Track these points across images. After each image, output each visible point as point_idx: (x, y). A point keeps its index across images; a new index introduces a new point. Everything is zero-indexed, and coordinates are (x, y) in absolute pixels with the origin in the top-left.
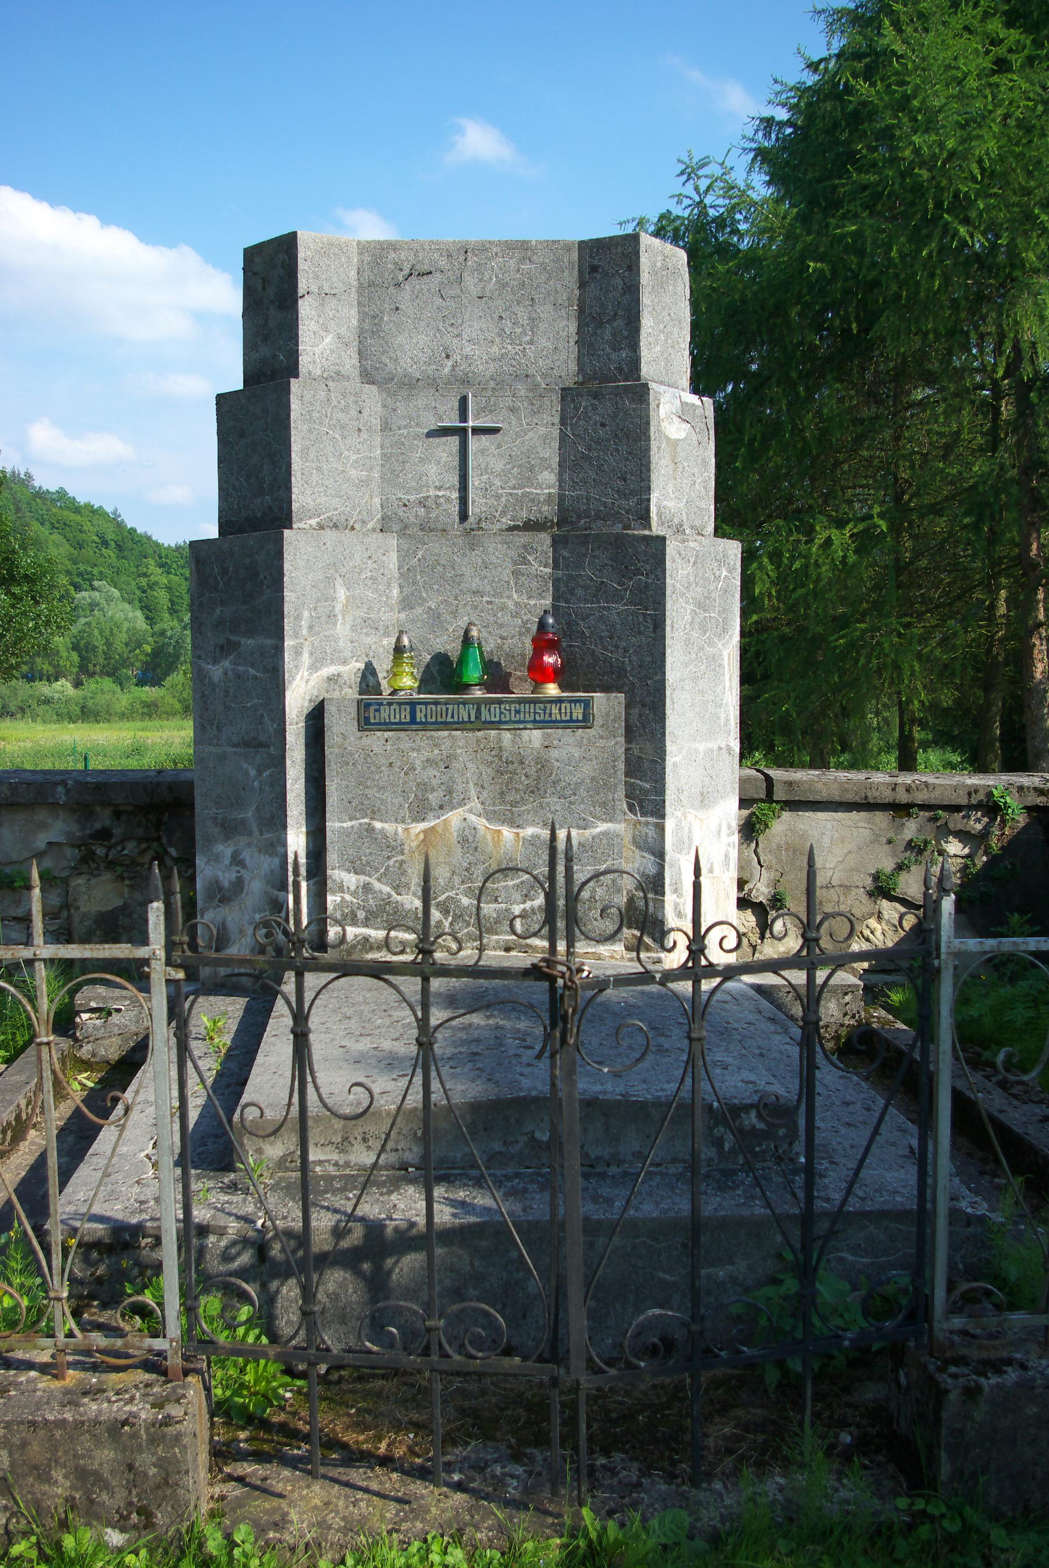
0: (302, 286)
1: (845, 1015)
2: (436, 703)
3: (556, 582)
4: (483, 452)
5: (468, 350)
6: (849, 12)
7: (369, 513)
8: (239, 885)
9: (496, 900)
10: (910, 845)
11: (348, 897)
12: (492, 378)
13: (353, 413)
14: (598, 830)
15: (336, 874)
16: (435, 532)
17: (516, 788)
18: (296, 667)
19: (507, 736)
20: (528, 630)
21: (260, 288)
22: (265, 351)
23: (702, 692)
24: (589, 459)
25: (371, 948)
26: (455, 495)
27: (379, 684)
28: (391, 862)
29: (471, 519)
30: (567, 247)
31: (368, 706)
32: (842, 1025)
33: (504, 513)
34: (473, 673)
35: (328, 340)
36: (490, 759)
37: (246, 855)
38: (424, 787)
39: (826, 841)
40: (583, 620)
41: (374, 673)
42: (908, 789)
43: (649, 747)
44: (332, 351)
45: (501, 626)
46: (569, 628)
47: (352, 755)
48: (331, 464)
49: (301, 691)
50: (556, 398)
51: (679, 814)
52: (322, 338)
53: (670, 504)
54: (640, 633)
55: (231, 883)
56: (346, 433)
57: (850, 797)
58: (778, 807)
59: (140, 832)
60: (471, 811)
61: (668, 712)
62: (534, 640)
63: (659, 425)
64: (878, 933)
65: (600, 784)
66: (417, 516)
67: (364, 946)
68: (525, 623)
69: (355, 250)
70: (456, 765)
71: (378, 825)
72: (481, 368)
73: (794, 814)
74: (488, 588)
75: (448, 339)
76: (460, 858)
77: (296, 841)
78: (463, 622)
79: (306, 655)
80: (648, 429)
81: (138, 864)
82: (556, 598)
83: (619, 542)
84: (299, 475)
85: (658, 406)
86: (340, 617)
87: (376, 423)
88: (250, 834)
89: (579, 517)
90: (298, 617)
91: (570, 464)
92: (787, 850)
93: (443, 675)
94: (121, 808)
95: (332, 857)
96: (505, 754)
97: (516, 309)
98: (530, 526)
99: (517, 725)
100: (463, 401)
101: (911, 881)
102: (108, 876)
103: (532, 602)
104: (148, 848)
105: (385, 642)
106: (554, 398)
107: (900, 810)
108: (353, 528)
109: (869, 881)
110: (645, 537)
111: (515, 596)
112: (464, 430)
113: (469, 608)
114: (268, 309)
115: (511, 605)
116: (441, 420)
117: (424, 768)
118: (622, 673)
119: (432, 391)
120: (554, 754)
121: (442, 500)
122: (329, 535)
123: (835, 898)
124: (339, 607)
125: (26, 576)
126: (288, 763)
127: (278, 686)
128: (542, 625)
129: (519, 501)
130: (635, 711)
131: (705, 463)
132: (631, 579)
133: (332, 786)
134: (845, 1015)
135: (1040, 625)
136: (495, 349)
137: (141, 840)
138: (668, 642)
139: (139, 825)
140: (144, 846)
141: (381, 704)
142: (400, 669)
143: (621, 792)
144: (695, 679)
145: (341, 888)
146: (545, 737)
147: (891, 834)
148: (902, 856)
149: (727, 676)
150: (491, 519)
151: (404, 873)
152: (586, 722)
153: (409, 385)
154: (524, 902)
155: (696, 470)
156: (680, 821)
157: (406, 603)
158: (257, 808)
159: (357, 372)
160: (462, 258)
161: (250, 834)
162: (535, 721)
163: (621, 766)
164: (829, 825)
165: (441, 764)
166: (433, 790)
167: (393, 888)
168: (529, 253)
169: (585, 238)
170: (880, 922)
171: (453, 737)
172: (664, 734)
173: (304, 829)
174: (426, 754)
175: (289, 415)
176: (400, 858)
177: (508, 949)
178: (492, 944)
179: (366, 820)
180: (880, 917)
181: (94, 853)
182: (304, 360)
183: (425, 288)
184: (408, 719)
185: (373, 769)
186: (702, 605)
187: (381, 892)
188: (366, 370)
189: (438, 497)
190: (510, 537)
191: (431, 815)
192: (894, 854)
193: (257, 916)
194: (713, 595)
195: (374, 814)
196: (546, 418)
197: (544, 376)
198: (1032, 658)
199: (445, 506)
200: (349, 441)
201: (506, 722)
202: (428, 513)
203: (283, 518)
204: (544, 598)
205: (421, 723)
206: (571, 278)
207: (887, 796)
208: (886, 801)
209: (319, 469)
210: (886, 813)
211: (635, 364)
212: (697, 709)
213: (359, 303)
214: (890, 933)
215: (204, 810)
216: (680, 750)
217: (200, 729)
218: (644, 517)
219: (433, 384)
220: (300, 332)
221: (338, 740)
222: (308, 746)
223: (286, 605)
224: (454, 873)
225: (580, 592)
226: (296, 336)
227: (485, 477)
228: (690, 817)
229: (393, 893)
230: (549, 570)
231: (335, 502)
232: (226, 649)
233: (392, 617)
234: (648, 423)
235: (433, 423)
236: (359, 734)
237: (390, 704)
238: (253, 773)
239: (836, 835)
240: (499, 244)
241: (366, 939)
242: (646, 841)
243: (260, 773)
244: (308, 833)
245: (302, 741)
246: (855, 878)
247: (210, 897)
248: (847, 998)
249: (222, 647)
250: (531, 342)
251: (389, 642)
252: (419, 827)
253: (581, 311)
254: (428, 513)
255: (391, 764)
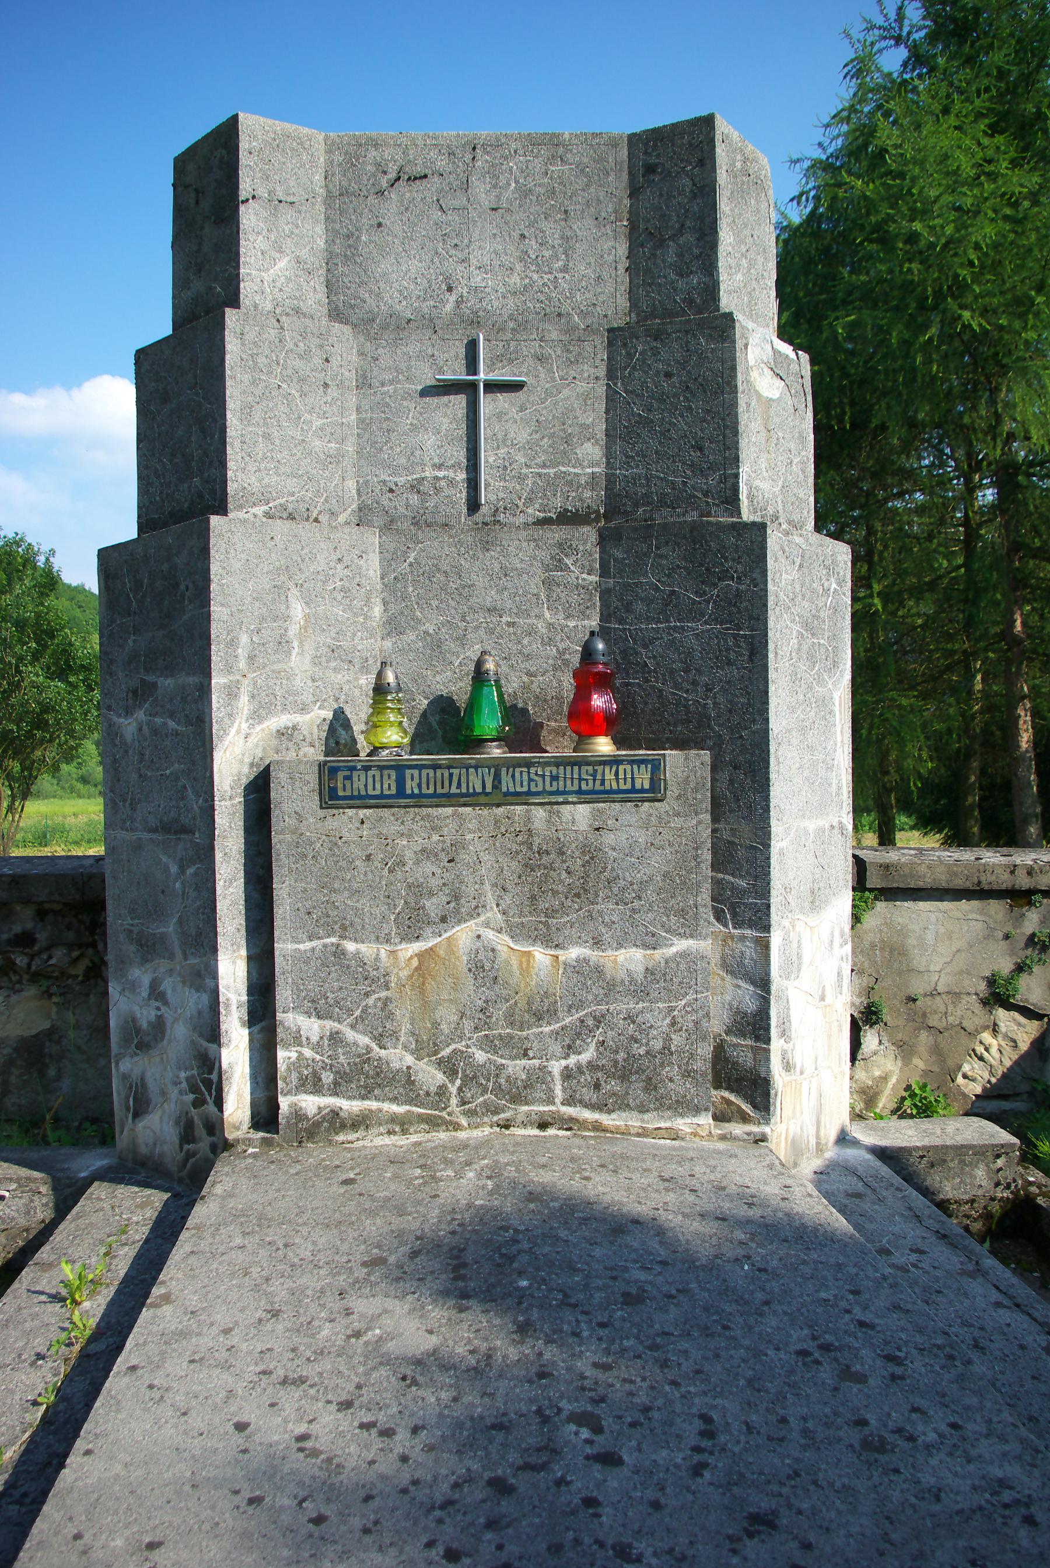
0: (245, 187)
1: (997, 1184)
2: (435, 767)
3: (605, 594)
4: (500, 416)
5: (478, 280)
6: (821, 162)
7: (340, 500)
8: (159, 1026)
9: (525, 1055)
10: (1031, 941)
11: (308, 1053)
12: (511, 317)
13: (317, 361)
14: (674, 950)
15: (291, 1018)
16: (432, 526)
17: (557, 890)
18: (230, 715)
19: (539, 814)
20: (566, 663)
21: (192, 202)
22: (198, 285)
23: (811, 748)
24: (648, 423)
25: (343, 1127)
26: (462, 476)
27: (354, 741)
28: (371, 1001)
29: (484, 510)
30: (613, 143)
31: (334, 771)
32: (993, 1199)
33: (530, 500)
34: (489, 723)
35: (282, 264)
36: (515, 847)
37: (167, 986)
38: (419, 890)
39: (930, 937)
40: (645, 646)
41: (347, 725)
42: (1030, 872)
43: (745, 827)
44: (289, 280)
45: (528, 657)
46: (625, 656)
47: (311, 844)
48: (285, 429)
49: (238, 750)
50: (600, 342)
51: (786, 923)
52: (275, 258)
53: (764, 485)
54: (729, 663)
55: (149, 1023)
56: (306, 388)
57: (959, 883)
58: (872, 896)
59: (70, 936)
60: (487, 925)
61: (773, 776)
62: (576, 675)
63: (748, 374)
64: (994, 1050)
65: (675, 883)
66: (407, 506)
67: (332, 1123)
68: (561, 653)
69: (322, 147)
70: (463, 857)
71: (350, 946)
72: (496, 304)
73: (890, 904)
74: (509, 604)
75: (451, 266)
76: (470, 992)
77: (232, 971)
78: (474, 653)
79: (244, 699)
80: (734, 377)
81: (69, 976)
82: (605, 617)
83: (696, 536)
84: (237, 444)
85: (746, 346)
86: (296, 644)
87: (350, 377)
88: (171, 957)
89: (636, 505)
90: (233, 643)
91: (621, 432)
92: (882, 949)
93: (446, 726)
94: (47, 906)
95: (283, 994)
96: (537, 841)
97: (544, 225)
98: (567, 518)
99: (554, 798)
100: (472, 347)
101: (1033, 985)
102: (31, 991)
103: (572, 624)
104: (82, 956)
105: (363, 681)
106: (598, 341)
107: (1020, 897)
108: (316, 520)
109: (982, 986)
110: (734, 526)
111: (547, 615)
112: (474, 385)
113: (481, 632)
114: (202, 228)
115: (541, 626)
116: (441, 371)
117: (417, 862)
118: (703, 720)
119: (429, 333)
120: (609, 839)
121: (443, 483)
122: (281, 528)
123: (942, 1009)
124: (293, 630)
125: (83, 666)
126: (219, 856)
127: (204, 745)
128: (588, 652)
129: (551, 483)
130: (725, 775)
131: (802, 439)
132: (715, 585)
133: (283, 890)
134: (997, 1184)
135: (1024, 697)
136: (515, 280)
137: (71, 947)
138: (772, 675)
139: (69, 927)
140: (75, 954)
141: (354, 768)
142: (382, 718)
143: (705, 896)
144: (803, 730)
145: (297, 1039)
146: (597, 814)
147: (1008, 928)
148: (1022, 954)
149: (838, 728)
150: (511, 508)
151: (390, 1016)
152: (655, 792)
153: (398, 327)
154: (566, 1057)
155: (792, 446)
156: (788, 934)
157: (393, 626)
158: (180, 922)
159: (325, 311)
160: (468, 157)
161: (171, 957)
162: (580, 792)
163: (707, 856)
164: (933, 917)
165: (442, 855)
166: (431, 894)
167: (374, 1038)
168: (561, 150)
169: (637, 130)
170: (995, 1037)
171: (460, 816)
172: (767, 809)
173: (244, 952)
174: (419, 843)
175: (223, 360)
176: (383, 994)
177: (543, 1126)
178: (520, 1118)
179: (333, 940)
180: (995, 1030)
181: (14, 964)
182: (246, 288)
183: (419, 197)
184: (393, 791)
185: (343, 864)
186: (810, 627)
187: (355, 1043)
188: (337, 308)
189: (437, 478)
190: (540, 532)
191: (429, 931)
192: (1012, 953)
193: (183, 1075)
194: (822, 614)
195: (344, 931)
196: (588, 370)
197: (583, 315)
198: (1018, 729)
199: (447, 492)
200: (310, 400)
201: (538, 794)
202: (424, 501)
203: (216, 500)
204: (589, 618)
205: (412, 796)
206: (618, 183)
207: (1004, 881)
208: (1004, 887)
209: (267, 436)
210: (1003, 902)
211: (712, 291)
212: (806, 773)
213: (327, 218)
214: (1007, 1050)
215: (117, 918)
216: (787, 830)
217: (112, 808)
218: (732, 500)
219: (431, 324)
220: (242, 250)
221: (291, 821)
222: (248, 830)
223: (213, 625)
224: (463, 1015)
225: (639, 607)
226: (237, 254)
227: (502, 451)
228: (800, 926)
229: (374, 1046)
230: (594, 578)
231: (291, 484)
232: (142, 693)
233: (373, 645)
234: (734, 368)
235: (428, 377)
236: (321, 813)
237: (366, 769)
238: (174, 869)
239: (942, 930)
240: (519, 137)
241: (335, 1113)
242: (741, 964)
243: (182, 870)
244: (250, 958)
245: (239, 823)
246: (966, 983)
247: (126, 1041)
248: (1000, 1162)
249: (135, 692)
250: (565, 269)
251: (367, 681)
252: (410, 949)
253: (633, 227)
254: (424, 501)
255: (368, 857)
